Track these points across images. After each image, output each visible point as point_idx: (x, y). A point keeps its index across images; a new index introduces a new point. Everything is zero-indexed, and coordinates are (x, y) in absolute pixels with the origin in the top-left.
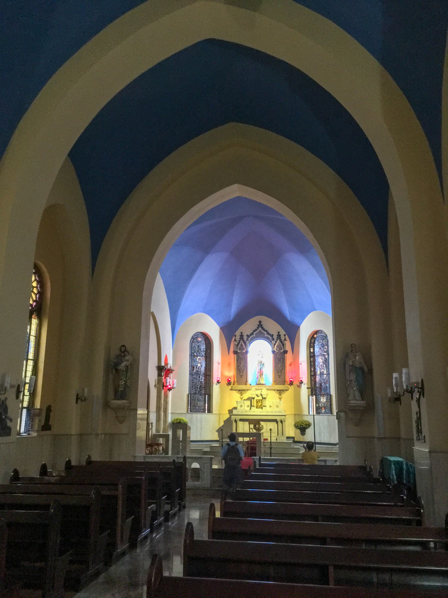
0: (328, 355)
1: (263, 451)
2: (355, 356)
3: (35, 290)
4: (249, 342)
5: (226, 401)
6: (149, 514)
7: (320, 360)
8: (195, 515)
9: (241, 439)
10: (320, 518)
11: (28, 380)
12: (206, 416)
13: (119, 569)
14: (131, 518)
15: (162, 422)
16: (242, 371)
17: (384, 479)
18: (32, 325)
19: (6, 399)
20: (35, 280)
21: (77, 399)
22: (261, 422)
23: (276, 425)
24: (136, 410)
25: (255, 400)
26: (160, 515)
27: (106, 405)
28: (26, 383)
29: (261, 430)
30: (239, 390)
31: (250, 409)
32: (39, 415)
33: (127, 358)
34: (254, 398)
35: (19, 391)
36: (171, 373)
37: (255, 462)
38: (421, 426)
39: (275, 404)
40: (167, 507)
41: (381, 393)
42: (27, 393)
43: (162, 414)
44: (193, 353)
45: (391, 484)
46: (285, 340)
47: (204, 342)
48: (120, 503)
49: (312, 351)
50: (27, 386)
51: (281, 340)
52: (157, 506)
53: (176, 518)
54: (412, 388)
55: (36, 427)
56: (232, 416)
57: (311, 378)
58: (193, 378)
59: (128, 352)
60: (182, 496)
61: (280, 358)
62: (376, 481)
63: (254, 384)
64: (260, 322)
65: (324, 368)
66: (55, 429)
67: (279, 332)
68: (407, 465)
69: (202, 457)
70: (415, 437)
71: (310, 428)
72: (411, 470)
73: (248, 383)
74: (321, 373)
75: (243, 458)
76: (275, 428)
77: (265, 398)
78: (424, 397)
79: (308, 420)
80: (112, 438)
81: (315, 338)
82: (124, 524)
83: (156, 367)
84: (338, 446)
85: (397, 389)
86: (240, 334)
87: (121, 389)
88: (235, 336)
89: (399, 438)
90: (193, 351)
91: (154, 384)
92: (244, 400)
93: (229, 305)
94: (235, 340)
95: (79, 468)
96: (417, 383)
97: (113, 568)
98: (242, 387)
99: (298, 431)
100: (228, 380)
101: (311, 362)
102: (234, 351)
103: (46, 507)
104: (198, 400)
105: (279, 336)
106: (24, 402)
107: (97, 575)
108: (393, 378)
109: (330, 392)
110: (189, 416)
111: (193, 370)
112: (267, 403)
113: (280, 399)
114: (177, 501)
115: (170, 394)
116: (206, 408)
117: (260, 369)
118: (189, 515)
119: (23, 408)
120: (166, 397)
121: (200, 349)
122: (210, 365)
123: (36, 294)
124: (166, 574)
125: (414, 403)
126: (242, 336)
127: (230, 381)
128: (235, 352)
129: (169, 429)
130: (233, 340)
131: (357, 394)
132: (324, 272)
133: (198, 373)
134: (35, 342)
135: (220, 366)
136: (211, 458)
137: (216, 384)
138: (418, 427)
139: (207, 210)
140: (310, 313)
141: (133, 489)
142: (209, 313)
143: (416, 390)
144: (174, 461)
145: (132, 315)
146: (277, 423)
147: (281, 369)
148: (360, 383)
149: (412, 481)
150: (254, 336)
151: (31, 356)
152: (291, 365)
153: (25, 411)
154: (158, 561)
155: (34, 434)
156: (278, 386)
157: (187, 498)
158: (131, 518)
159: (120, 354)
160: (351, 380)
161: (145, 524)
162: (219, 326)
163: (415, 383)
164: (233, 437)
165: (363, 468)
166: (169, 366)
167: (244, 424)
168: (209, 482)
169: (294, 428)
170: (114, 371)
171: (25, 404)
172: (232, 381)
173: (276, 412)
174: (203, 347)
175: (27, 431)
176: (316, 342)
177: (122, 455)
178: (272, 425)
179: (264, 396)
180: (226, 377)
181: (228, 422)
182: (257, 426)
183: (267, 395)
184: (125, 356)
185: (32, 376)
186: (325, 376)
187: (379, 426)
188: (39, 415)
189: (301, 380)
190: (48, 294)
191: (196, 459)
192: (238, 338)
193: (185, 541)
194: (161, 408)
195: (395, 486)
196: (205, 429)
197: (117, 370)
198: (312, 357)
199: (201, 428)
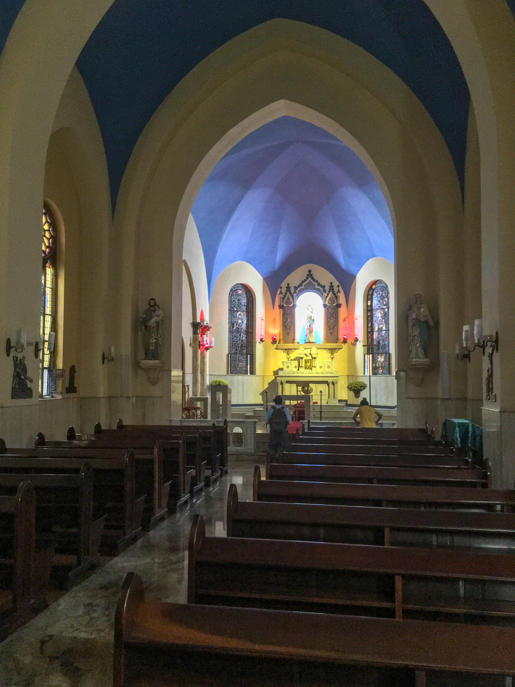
0: (388, 308)
1: (312, 415)
2: (419, 309)
3: (47, 235)
4: (297, 295)
5: (270, 361)
6: (188, 479)
7: (378, 315)
8: (238, 480)
9: (287, 402)
10: (375, 481)
11: (47, 338)
12: (248, 378)
13: (158, 534)
14: (169, 483)
15: (199, 385)
16: (288, 327)
17: (447, 442)
18: (47, 275)
19: (24, 357)
20: (47, 222)
21: (104, 358)
22: (310, 384)
23: (327, 387)
24: (170, 371)
25: (303, 360)
26: (200, 481)
27: (136, 365)
28: (44, 341)
29: (310, 393)
30: (286, 349)
31: (298, 370)
32: (62, 376)
33: (158, 313)
34: (302, 358)
35: (37, 350)
36: (208, 330)
37: (303, 425)
38: (492, 384)
39: (326, 364)
40: (208, 473)
41: (448, 349)
42: (47, 352)
43: (199, 375)
44: (233, 308)
45: (454, 447)
46: (339, 291)
47: (245, 295)
48: (156, 466)
49: (369, 304)
50: (46, 345)
51: (333, 292)
52: (196, 472)
53: (218, 483)
54: (484, 342)
55: (60, 390)
56: (278, 378)
57: (367, 335)
58: (233, 336)
59: (158, 306)
60: (223, 462)
61: (333, 313)
62: (438, 443)
63: (302, 342)
64: (310, 271)
65: (383, 323)
66: (81, 392)
67: (331, 283)
68: (473, 426)
69: (245, 421)
70: (484, 397)
71: (365, 390)
72: (477, 433)
73: (296, 341)
74: (379, 329)
75: (290, 422)
76: (325, 390)
77: (315, 358)
78: (497, 351)
79: (363, 381)
80: (143, 401)
81: (374, 290)
82: (161, 489)
83: (191, 324)
84: (396, 409)
85: (467, 344)
86: (287, 286)
87: (151, 348)
88: (281, 288)
89: (466, 399)
90: (232, 306)
91: (189, 343)
92: (291, 360)
93: (273, 252)
94: (281, 293)
95: (110, 432)
96: (491, 336)
97: (151, 533)
98: (290, 346)
99: (352, 393)
100: (273, 338)
101: (368, 317)
102: (279, 305)
103: (77, 471)
104: (239, 360)
105: (331, 287)
106: (45, 362)
107: (134, 540)
108: (462, 332)
109: (389, 350)
110: (229, 378)
111: (233, 327)
112: (317, 363)
113: (332, 358)
114: (218, 467)
115: (208, 353)
116: (249, 369)
117: (310, 326)
118: (231, 481)
119: (44, 368)
120: (203, 357)
121: (241, 304)
122: (253, 321)
123: (49, 239)
124: (208, 535)
125: (486, 359)
126: (288, 288)
127: (275, 339)
128: (281, 307)
129: (207, 392)
130: (279, 292)
131: (420, 351)
132: (387, 209)
133: (238, 331)
134: (52, 295)
135: (263, 322)
136: (255, 422)
137: (260, 343)
138: (489, 386)
139: (246, 134)
140: (368, 260)
141: (170, 455)
142: (250, 261)
143: (489, 344)
144: (214, 424)
145: (161, 262)
146: (328, 385)
147: (333, 325)
148: (424, 337)
149: (478, 445)
150: (303, 287)
151: (48, 311)
152: (344, 320)
153: (46, 372)
154: (199, 523)
155: (59, 397)
156: (330, 344)
157: (229, 464)
158: (169, 483)
159: (149, 309)
160: (414, 336)
161: (184, 489)
162: (263, 277)
163: (487, 336)
164: (279, 400)
165: (423, 431)
166: (205, 322)
167: (291, 386)
168: (252, 447)
169: (347, 390)
170: (143, 327)
171: (46, 364)
172: (278, 338)
173: (326, 373)
174: (244, 301)
175: (50, 393)
176: (375, 294)
177: (157, 419)
178: (323, 387)
179: (313, 356)
180: (271, 334)
181: (273, 384)
182: (306, 388)
183: (317, 354)
184: (155, 310)
185: (52, 333)
186: (384, 332)
187: (443, 385)
188: (62, 376)
189: (356, 338)
190: (63, 239)
191: (238, 424)
192: (284, 290)
193: (229, 503)
194: (198, 369)
195: (458, 449)
196: (247, 392)
197: (146, 327)
198: (369, 311)
199: (243, 391)
